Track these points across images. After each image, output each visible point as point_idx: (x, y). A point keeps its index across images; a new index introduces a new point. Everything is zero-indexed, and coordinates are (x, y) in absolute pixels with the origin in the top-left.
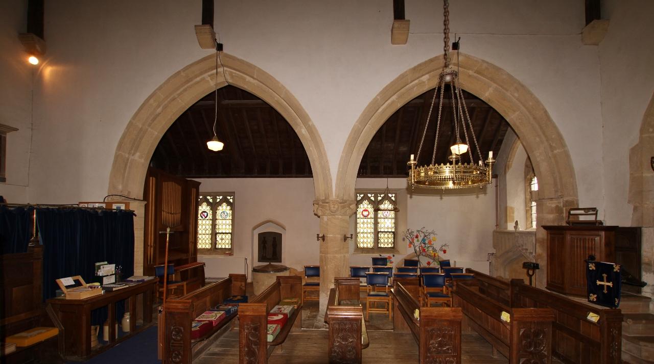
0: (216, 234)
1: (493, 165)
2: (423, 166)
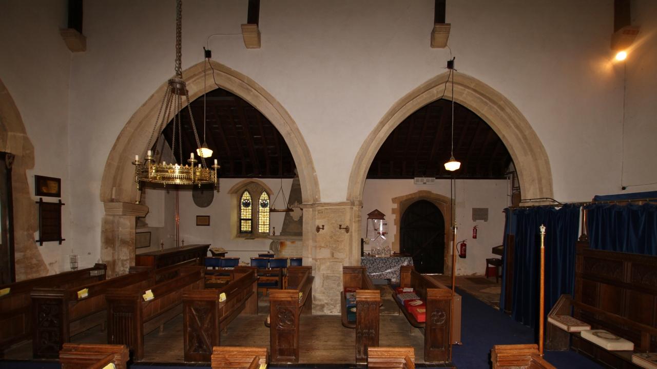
0: (241, 220)
1: (217, 169)
2: (179, 164)
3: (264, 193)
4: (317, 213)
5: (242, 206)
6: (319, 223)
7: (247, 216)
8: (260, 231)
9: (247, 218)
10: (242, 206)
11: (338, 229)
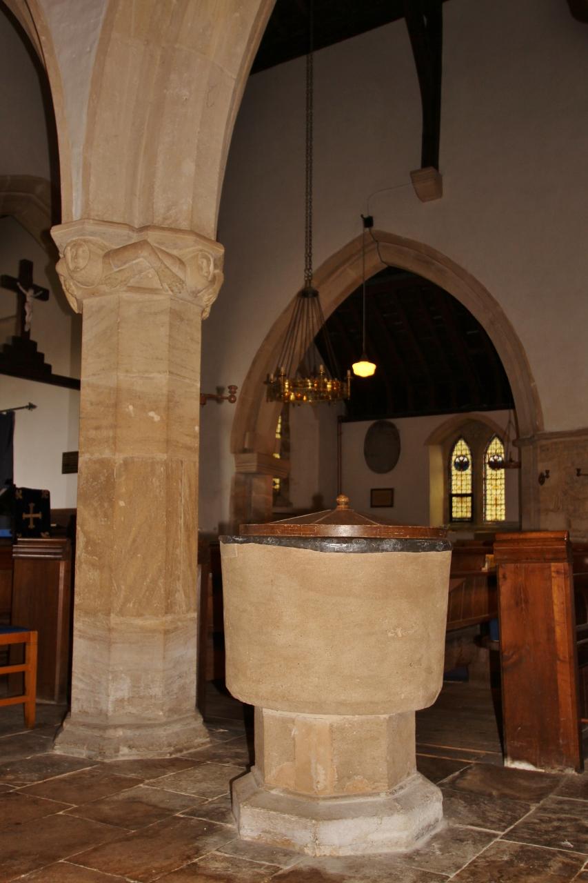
0: (451, 496)
3: (495, 441)
4: (539, 451)
5: (453, 468)
6: (541, 468)
7: (464, 487)
8: (489, 518)
9: (464, 492)
10: (453, 468)
11: (575, 477)
